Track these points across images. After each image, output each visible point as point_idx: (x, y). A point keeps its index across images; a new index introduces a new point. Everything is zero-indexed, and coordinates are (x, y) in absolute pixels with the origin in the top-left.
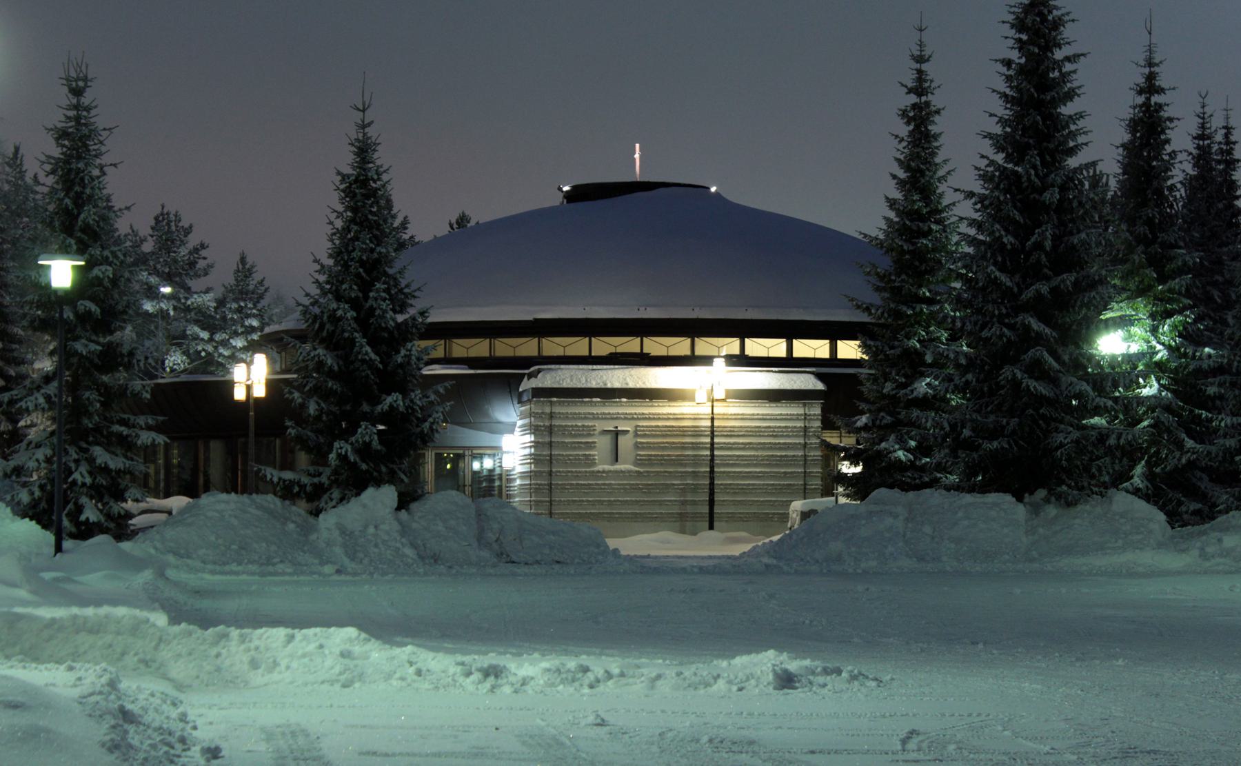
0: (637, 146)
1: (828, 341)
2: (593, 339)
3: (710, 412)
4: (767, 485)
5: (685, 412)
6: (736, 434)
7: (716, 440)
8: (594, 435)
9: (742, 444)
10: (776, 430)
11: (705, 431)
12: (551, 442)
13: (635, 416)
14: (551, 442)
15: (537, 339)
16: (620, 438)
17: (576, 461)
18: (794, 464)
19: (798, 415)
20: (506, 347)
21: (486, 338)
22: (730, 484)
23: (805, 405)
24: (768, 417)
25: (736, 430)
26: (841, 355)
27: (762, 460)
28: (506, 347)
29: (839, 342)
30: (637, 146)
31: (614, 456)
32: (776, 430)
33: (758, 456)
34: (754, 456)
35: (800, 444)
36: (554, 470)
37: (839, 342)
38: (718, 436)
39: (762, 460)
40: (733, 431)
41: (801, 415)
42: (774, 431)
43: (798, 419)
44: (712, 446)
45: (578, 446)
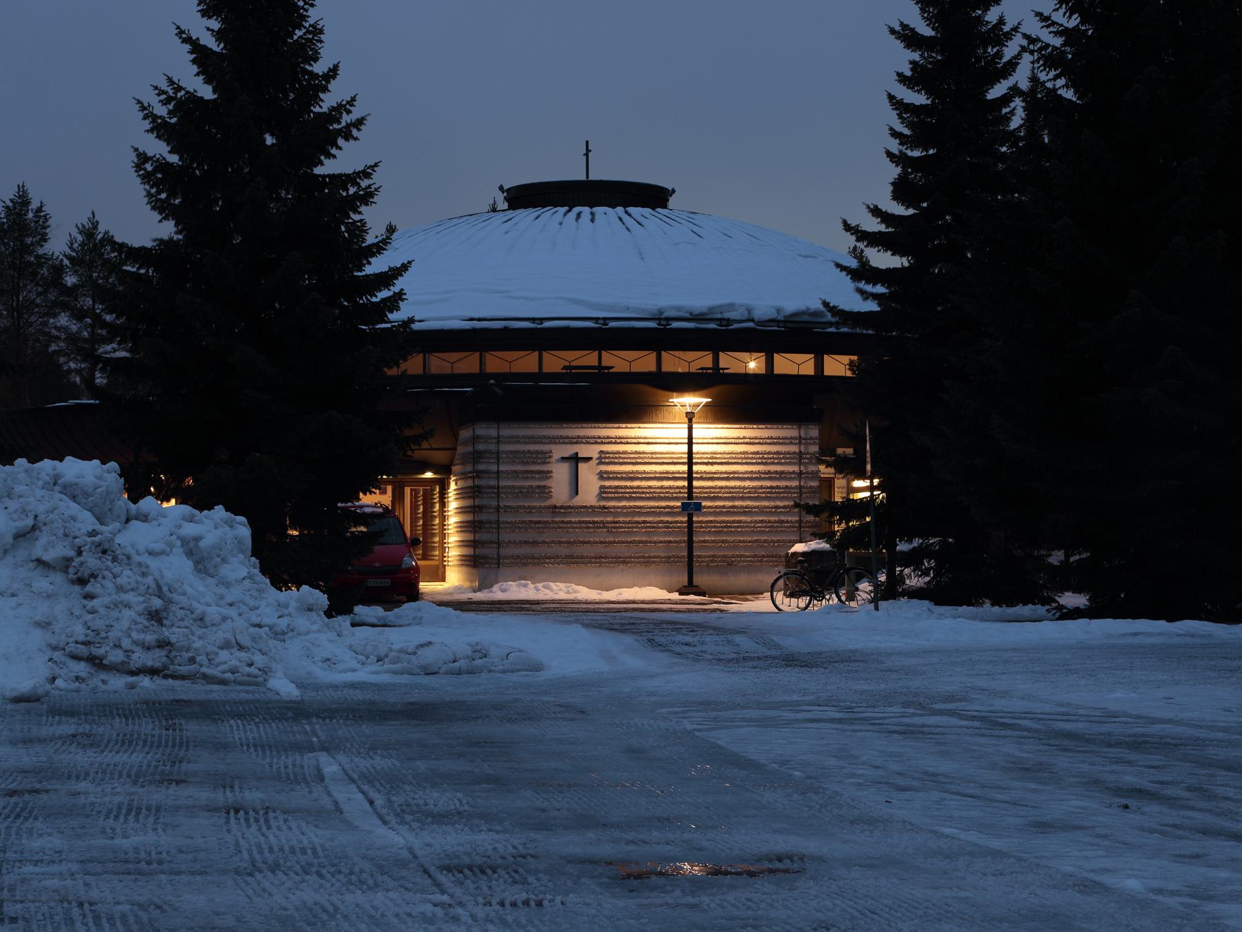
0: (97, 402)
1: (813, 356)
2: (544, 353)
3: (686, 435)
4: (756, 522)
5: (648, 436)
6: (718, 461)
7: (695, 468)
8: (549, 463)
9: (726, 473)
10: (766, 456)
11: (681, 458)
12: (498, 471)
13: (599, 440)
14: (498, 471)
15: (478, 354)
16: (582, 466)
17: (529, 493)
18: (787, 497)
19: (791, 438)
20: (620, 361)
21: (476, 351)
22: (711, 522)
23: (799, 428)
24: (756, 441)
25: (718, 456)
26: (666, 368)
27: (749, 492)
28: (620, 361)
29: (826, 356)
30: (97, 402)
31: (1012, 619)
32: (766, 456)
33: (744, 488)
34: (739, 487)
35: (794, 472)
36: (501, 505)
37: (826, 356)
38: (697, 463)
39: (749, 492)
40: (716, 458)
41: (795, 438)
42: (763, 458)
43: (791, 443)
44: (690, 477)
45: (528, 474)
